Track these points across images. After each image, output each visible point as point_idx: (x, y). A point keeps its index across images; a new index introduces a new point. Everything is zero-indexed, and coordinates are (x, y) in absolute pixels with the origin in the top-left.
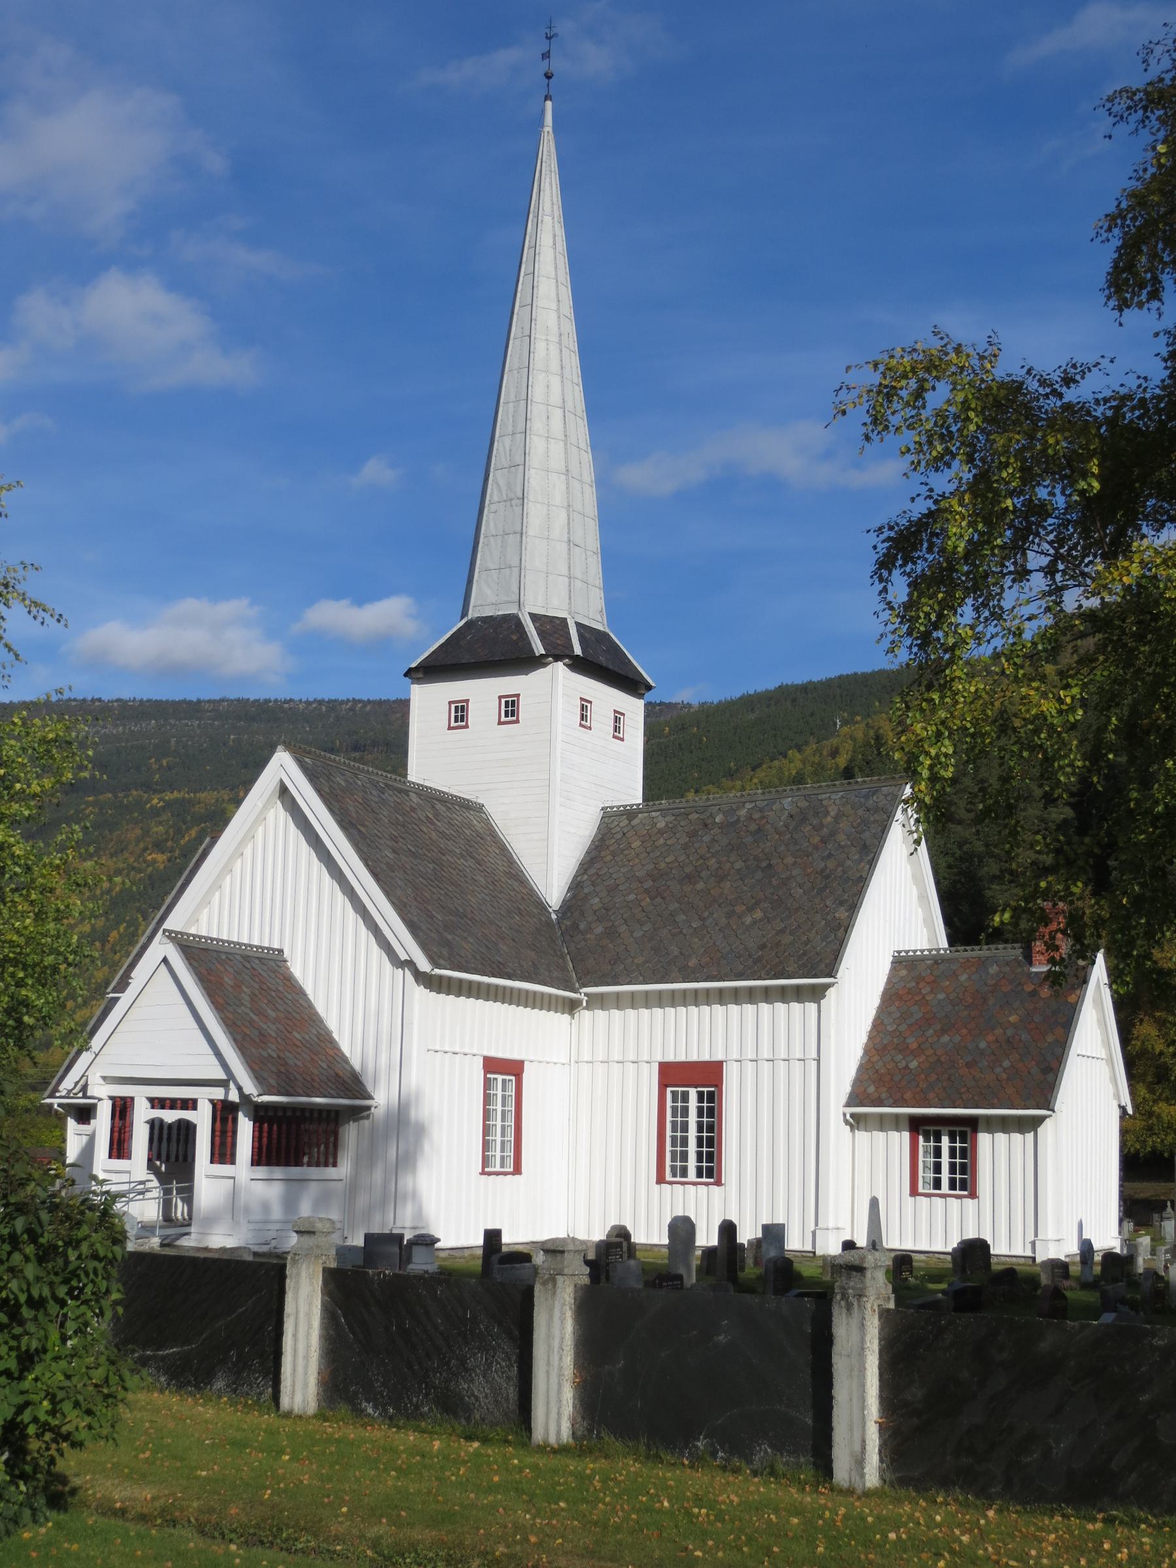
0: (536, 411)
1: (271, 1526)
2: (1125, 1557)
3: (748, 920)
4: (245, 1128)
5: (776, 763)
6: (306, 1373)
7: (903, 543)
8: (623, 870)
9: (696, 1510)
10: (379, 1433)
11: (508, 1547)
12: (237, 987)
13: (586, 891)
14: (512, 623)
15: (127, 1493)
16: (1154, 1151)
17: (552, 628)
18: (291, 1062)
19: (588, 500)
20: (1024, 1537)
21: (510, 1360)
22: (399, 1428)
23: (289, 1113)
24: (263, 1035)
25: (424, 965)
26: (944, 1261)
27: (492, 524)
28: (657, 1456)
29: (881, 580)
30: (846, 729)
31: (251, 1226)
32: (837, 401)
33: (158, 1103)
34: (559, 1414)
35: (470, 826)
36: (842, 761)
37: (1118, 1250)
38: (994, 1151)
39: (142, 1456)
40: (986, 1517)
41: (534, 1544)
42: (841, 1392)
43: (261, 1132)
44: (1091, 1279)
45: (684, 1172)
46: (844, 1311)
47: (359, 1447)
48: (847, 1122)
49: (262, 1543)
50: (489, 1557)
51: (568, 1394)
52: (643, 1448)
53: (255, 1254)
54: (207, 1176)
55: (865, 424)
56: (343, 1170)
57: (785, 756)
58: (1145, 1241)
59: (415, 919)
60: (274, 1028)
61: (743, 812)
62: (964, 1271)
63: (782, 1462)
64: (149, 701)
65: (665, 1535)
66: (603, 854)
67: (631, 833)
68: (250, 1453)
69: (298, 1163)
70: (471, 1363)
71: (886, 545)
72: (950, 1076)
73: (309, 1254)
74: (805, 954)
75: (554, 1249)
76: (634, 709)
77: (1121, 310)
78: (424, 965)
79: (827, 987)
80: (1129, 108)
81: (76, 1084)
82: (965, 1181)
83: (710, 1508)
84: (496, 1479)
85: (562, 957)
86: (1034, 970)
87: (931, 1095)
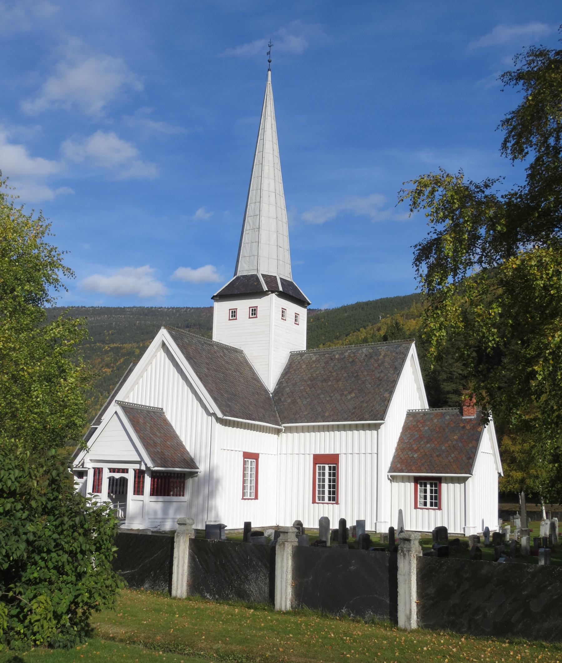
0: (264, 194)
1: (174, 644)
2: (520, 658)
3: (349, 397)
4: (148, 480)
5: (355, 333)
6: (182, 581)
7: (424, 252)
8: (299, 377)
9: (345, 638)
10: (212, 606)
11: (271, 653)
12: (145, 423)
13: (284, 385)
14: (255, 278)
15: (115, 630)
16: (510, 491)
17: (271, 280)
18: (166, 454)
19: (284, 229)
20: (478, 649)
21: (265, 576)
22: (220, 604)
23: (165, 475)
24: (155, 443)
25: (220, 415)
26: (428, 535)
27: (246, 238)
28: (326, 615)
29: (417, 266)
30: (383, 320)
31: (150, 520)
32: (399, 196)
33: (112, 470)
34: (286, 598)
35: (238, 359)
36: (382, 333)
37: (498, 531)
38: (448, 490)
39: (119, 615)
40: (461, 641)
41: (282, 652)
42: (401, 590)
43: (154, 482)
44: (488, 543)
45: (323, 499)
46: (402, 557)
47: (206, 612)
48: (389, 479)
49: (171, 651)
50: (264, 657)
51: (290, 590)
52: (320, 612)
53: (152, 532)
54: (132, 500)
55: (410, 205)
56: (187, 497)
57: (359, 331)
58: (508, 527)
59: (216, 396)
60: (159, 440)
61: (347, 354)
62: (437, 540)
63: (377, 618)
64: (104, 307)
65: (334, 648)
66: (291, 370)
67: (302, 362)
68: (162, 614)
69: (169, 495)
70: (249, 578)
71: (418, 252)
72: (430, 461)
73: (183, 533)
74: (372, 411)
75: (279, 532)
76: (303, 312)
77: (513, 160)
78: (220, 415)
79: (381, 424)
80: (510, 79)
81: (80, 462)
82: (436, 503)
83: (351, 637)
84: (263, 625)
85: (274, 411)
86: (464, 418)
87: (422, 468)
